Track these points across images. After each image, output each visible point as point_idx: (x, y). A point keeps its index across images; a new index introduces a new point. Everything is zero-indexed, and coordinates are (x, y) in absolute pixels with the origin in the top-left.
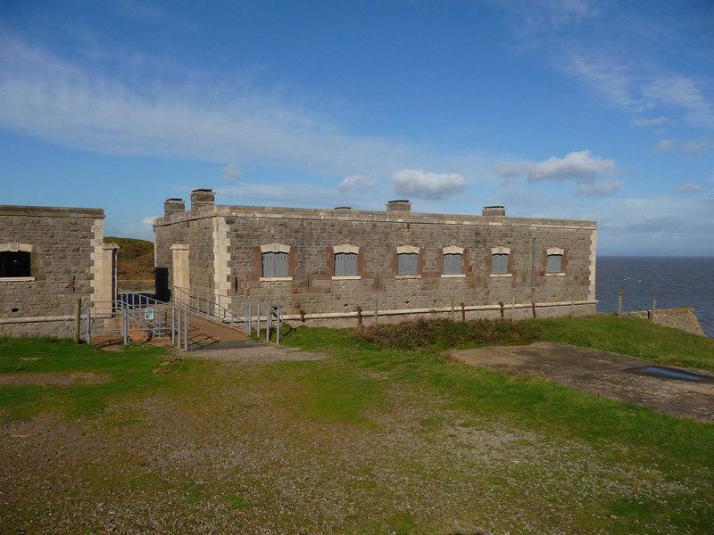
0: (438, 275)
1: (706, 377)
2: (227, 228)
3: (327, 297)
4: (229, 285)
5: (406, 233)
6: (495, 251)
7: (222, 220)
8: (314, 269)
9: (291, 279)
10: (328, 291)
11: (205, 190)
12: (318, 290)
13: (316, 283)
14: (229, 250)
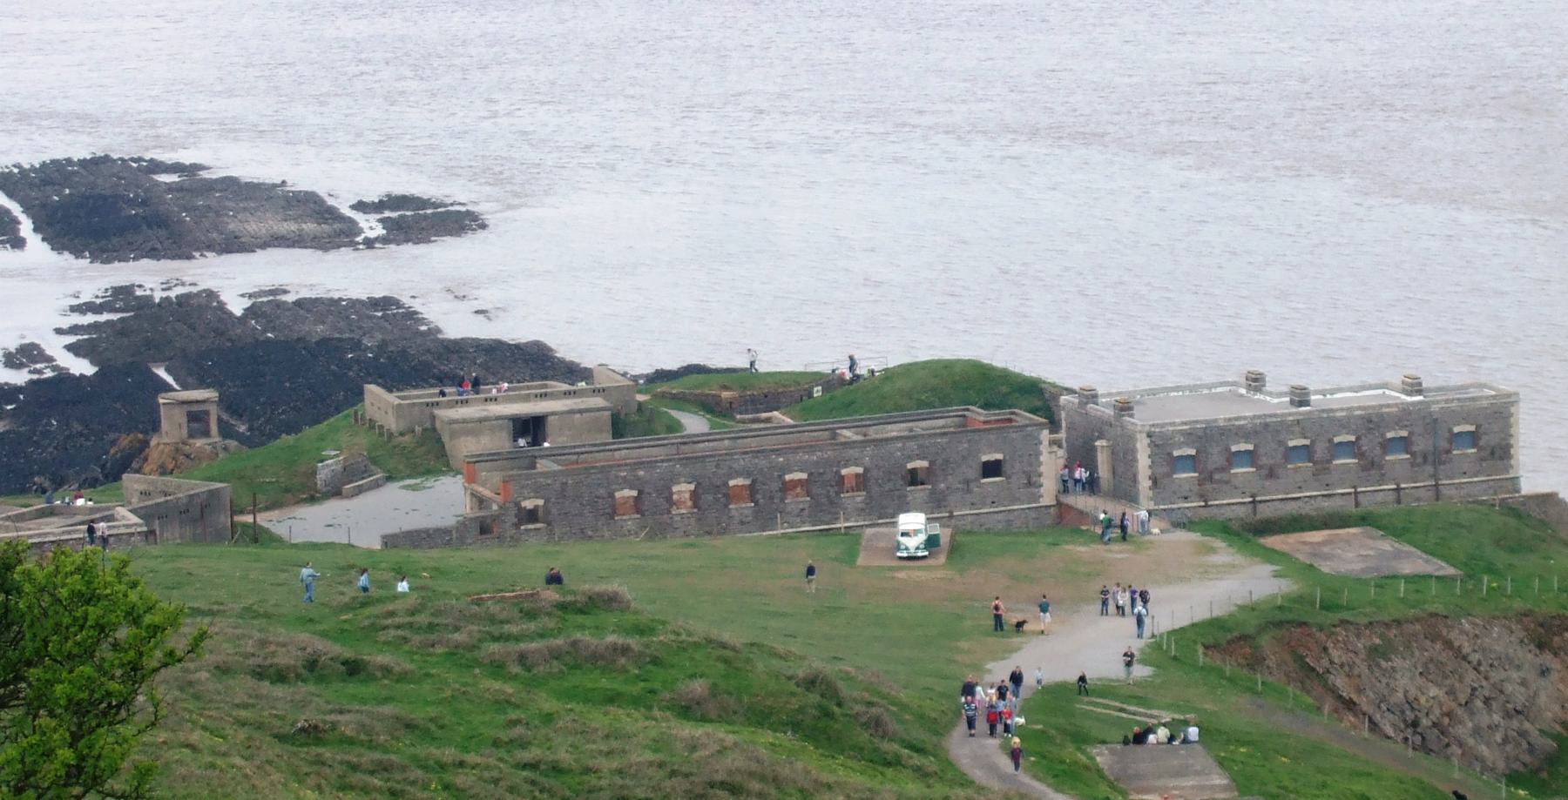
0: (1329, 461)
2: (1148, 440)
4: (1150, 483)
6: (1390, 435)
10: (1227, 483)
12: (1219, 482)
13: (1217, 476)
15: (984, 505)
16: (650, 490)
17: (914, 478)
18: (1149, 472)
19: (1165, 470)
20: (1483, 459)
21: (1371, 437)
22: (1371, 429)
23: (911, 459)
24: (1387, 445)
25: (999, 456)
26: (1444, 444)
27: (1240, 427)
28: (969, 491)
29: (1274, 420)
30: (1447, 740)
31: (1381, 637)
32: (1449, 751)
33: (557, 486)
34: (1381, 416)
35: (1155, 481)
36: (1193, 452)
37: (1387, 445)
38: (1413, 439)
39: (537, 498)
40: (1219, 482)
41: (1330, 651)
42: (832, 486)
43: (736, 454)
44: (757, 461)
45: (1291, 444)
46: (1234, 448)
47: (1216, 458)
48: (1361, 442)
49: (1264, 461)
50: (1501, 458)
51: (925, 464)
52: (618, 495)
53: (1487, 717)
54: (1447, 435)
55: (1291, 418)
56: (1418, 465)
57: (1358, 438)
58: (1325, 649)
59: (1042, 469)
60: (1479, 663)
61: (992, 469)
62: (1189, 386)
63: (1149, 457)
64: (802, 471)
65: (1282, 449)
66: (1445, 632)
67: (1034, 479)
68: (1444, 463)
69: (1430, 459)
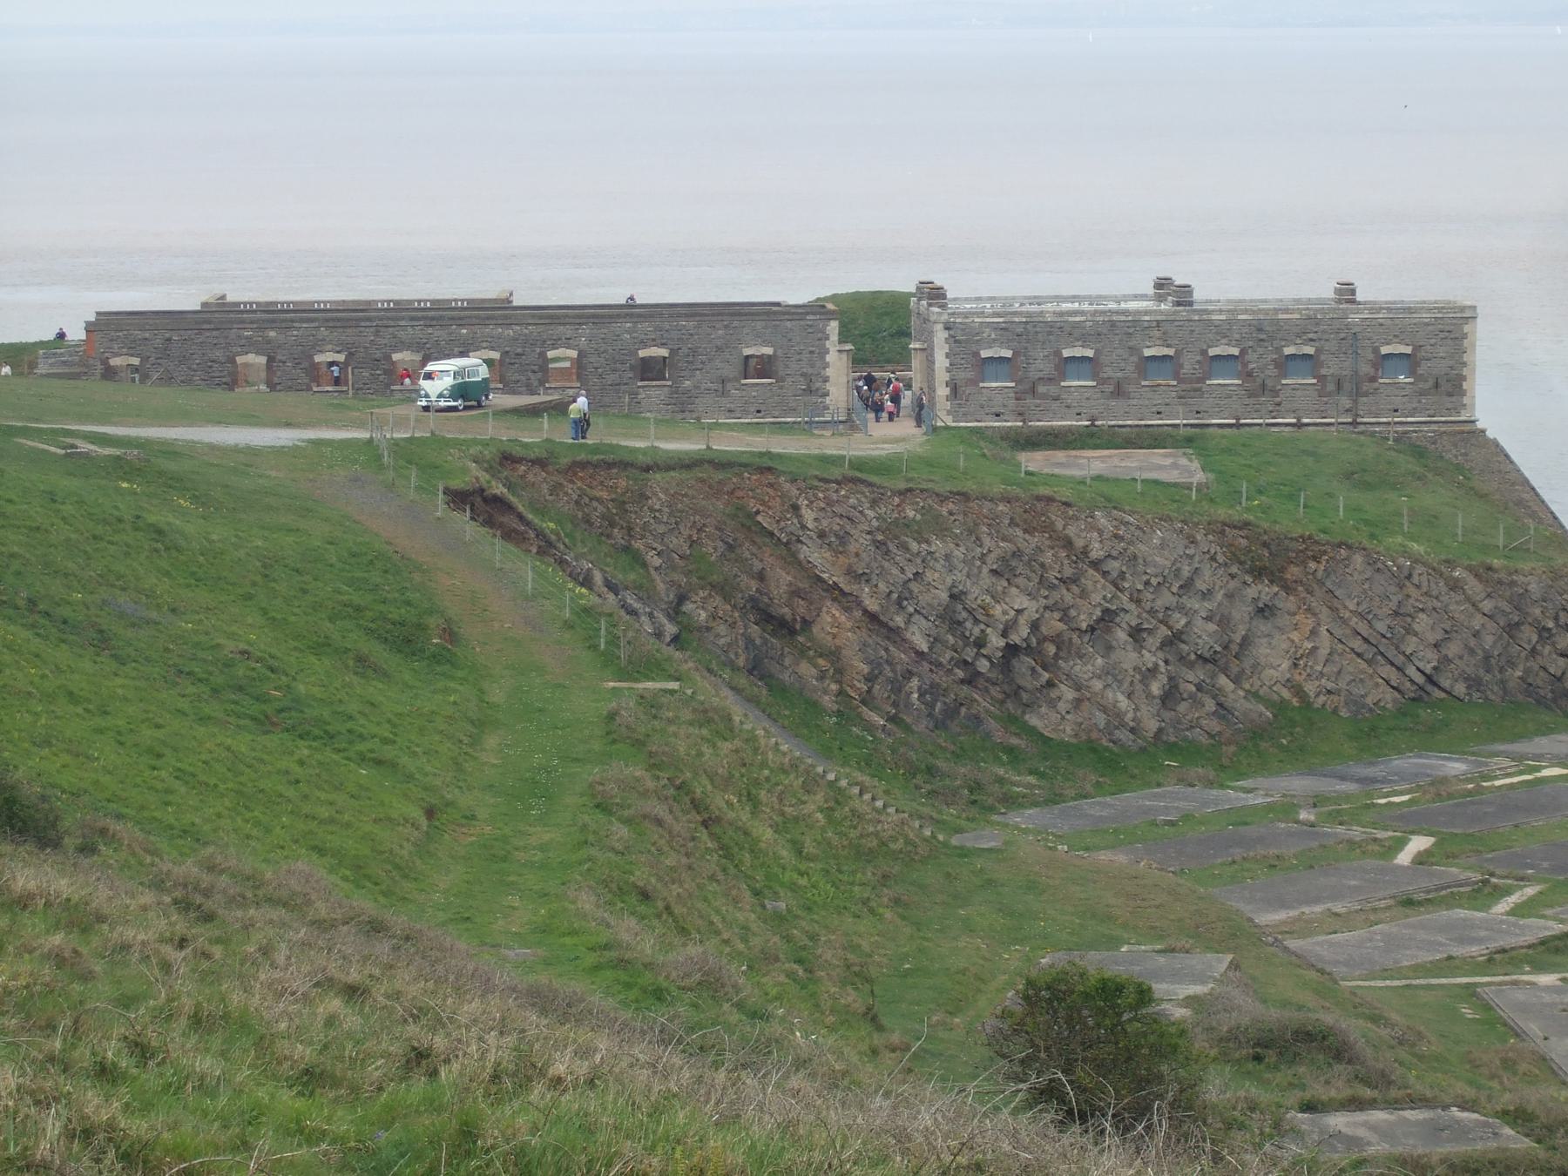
0: (1202, 380)
1: (1461, 886)
2: (946, 334)
3: (1055, 405)
4: (947, 391)
5: (1157, 333)
6: (1288, 351)
7: (939, 327)
8: (1041, 375)
9: (1013, 384)
10: (1056, 399)
11: (362, 311)
12: (1044, 397)
13: (1041, 389)
14: (947, 356)
15: (746, 413)
16: (284, 358)
17: (649, 370)
18: (946, 377)
19: (970, 375)
20: (1422, 393)
21: (1261, 350)
22: (1262, 340)
23: (645, 345)
24: (1286, 364)
25: (768, 351)
26: (1365, 369)
27: (1076, 325)
28: (724, 393)
29: (1123, 318)
30: (1046, 675)
31: (923, 511)
32: (1054, 694)
33: (158, 342)
34: (1276, 323)
35: (955, 389)
36: (1008, 354)
37: (1286, 364)
38: (1323, 357)
39: (132, 355)
40: (1044, 397)
41: (803, 511)
42: (534, 372)
43: (403, 319)
44: (430, 330)
45: (1148, 353)
46: (1066, 353)
47: (1041, 365)
48: (1247, 358)
49: (1108, 372)
50: (1450, 395)
51: (664, 352)
52: (240, 360)
53: (1135, 655)
54: (1371, 356)
55: (1147, 318)
56: (1330, 394)
57: (1243, 352)
58: (796, 508)
59: (829, 372)
60: (1122, 575)
61: (764, 368)
62: (1090, 296)
63: (947, 357)
64: (492, 349)
65: (1135, 359)
66: (1059, 525)
67: (818, 385)
68: (1366, 394)
69: (1347, 386)
